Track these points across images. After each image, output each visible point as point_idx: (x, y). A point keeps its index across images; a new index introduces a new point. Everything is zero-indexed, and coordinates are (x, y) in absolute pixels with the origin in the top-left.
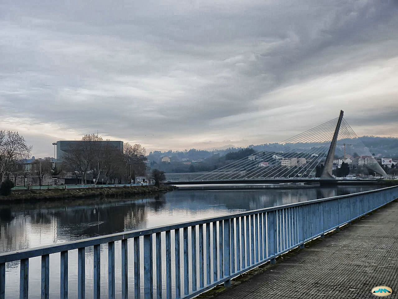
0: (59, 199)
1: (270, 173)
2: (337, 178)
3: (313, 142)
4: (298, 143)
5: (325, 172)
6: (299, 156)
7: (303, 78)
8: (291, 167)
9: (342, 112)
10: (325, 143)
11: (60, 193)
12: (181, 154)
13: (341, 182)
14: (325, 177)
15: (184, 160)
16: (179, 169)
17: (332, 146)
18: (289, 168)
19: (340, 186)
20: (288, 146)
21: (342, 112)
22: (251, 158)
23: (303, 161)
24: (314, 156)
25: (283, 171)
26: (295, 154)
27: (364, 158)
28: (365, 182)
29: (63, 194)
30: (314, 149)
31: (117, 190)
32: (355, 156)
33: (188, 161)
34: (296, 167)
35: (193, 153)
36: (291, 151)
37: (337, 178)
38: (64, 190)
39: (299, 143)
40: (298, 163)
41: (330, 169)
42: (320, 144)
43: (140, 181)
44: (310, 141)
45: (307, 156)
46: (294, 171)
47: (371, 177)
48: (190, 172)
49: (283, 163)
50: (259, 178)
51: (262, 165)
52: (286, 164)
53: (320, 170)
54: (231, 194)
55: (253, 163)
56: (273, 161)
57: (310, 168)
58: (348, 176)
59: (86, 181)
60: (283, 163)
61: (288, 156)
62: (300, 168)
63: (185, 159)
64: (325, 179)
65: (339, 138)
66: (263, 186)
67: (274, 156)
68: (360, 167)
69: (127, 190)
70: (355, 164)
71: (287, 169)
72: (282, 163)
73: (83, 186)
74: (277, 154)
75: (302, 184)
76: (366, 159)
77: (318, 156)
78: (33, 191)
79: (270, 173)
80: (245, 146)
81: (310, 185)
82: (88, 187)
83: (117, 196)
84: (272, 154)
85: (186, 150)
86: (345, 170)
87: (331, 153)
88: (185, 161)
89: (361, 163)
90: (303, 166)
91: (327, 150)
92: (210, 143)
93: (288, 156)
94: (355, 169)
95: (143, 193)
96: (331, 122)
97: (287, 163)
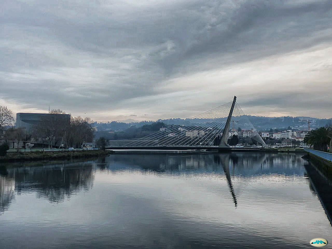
0: (40, 159)
1: (177, 141)
2: (231, 147)
3: (219, 117)
4: (201, 119)
5: (222, 141)
6: (199, 129)
7: (185, 73)
8: (193, 137)
9: (235, 97)
10: (222, 119)
11: (41, 155)
12: (105, 125)
13: (234, 149)
14: (222, 146)
15: (108, 129)
16: (116, 137)
17: (227, 123)
18: (192, 138)
19: (233, 153)
20: (188, 121)
21: (235, 97)
22: (162, 130)
23: (203, 133)
24: (209, 129)
25: (188, 140)
26: (194, 127)
27: (247, 131)
28: (242, 149)
29: (43, 155)
30: (208, 124)
31: (79, 153)
32: (239, 130)
33: (111, 131)
34: (197, 138)
35: (114, 124)
36: (190, 125)
37: (231, 147)
38: (43, 152)
39: (196, 118)
40: (198, 134)
41: (226, 140)
42: (212, 120)
43: (89, 147)
44: (211, 118)
45: (205, 129)
46: (196, 140)
47: (254, 146)
48: (114, 140)
49: (187, 134)
50: (171, 146)
51: (170, 135)
52: (190, 135)
53: (218, 141)
54: (147, 158)
55: (164, 133)
56: (179, 132)
57: (208, 139)
58: (238, 145)
59: (51, 146)
60: (187, 134)
61: (191, 128)
62: (200, 138)
63: (108, 129)
64: (223, 147)
65: (233, 115)
66: (174, 152)
67: (179, 129)
68: (244, 138)
69: (84, 153)
70: (241, 136)
71: (190, 139)
72: (186, 134)
73: (49, 150)
74: (181, 127)
75: (205, 150)
76: (248, 133)
77: (212, 129)
78: (21, 153)
79: (177, 141)
80: (155, 120)
81: (210, 151)
82: (59, 151)
83: (80, 157)
84: (178, 126)
85: (109, 122)
86: (234, 140)
87: (227, 128)
88: (109, 131)
89: (245, 135)
90: (202, 137)
91: (224, 126)
92: (121, 116)
93: (191, 128)
94: (244, 141)
95: (88, 156)
96: (225, 105)
97: (189, 134)
